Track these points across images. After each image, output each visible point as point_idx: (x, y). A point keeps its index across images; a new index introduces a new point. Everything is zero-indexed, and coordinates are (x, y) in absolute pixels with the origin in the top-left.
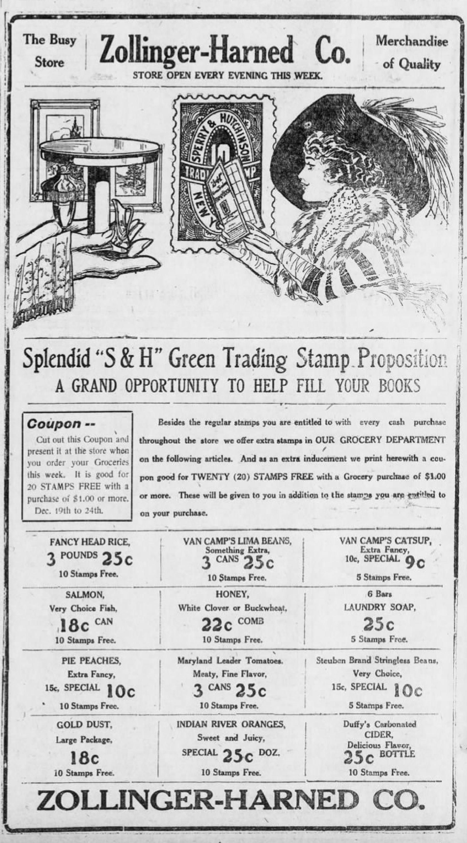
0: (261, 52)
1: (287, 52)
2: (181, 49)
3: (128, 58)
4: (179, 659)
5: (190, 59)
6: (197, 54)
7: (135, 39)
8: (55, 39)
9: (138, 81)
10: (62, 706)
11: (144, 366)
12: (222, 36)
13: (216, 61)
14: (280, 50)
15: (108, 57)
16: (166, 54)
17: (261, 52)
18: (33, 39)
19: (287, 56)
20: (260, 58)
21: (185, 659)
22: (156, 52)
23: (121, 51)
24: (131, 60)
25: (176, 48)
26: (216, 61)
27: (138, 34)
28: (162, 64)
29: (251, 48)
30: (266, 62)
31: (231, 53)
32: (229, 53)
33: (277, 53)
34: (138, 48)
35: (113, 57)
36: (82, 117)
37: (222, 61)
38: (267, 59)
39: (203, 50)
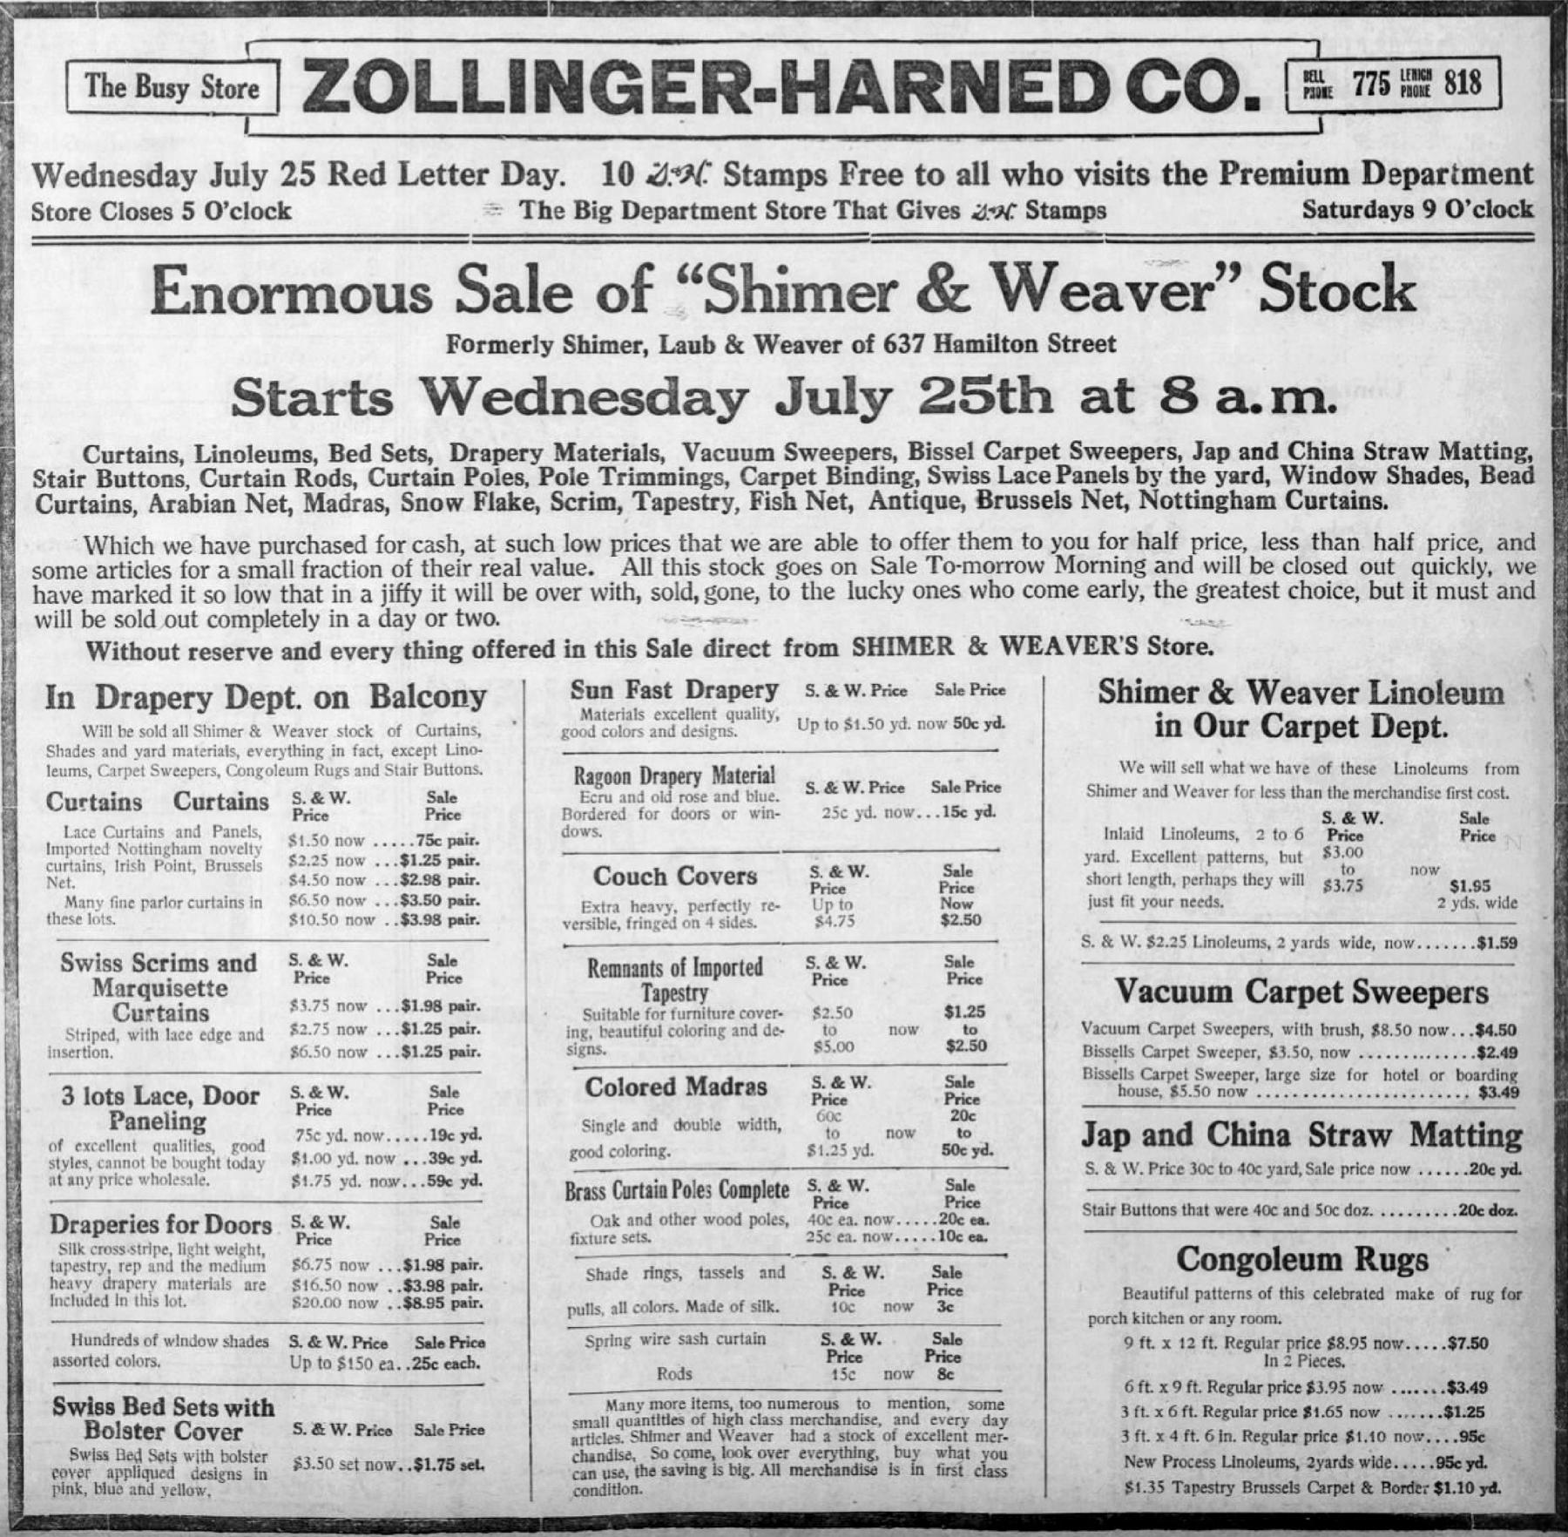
7: (981, 168)
8: (384, 695)
11: (564, 413)
18: (105, 84)
36: (71, 66)
37: (575, 413)
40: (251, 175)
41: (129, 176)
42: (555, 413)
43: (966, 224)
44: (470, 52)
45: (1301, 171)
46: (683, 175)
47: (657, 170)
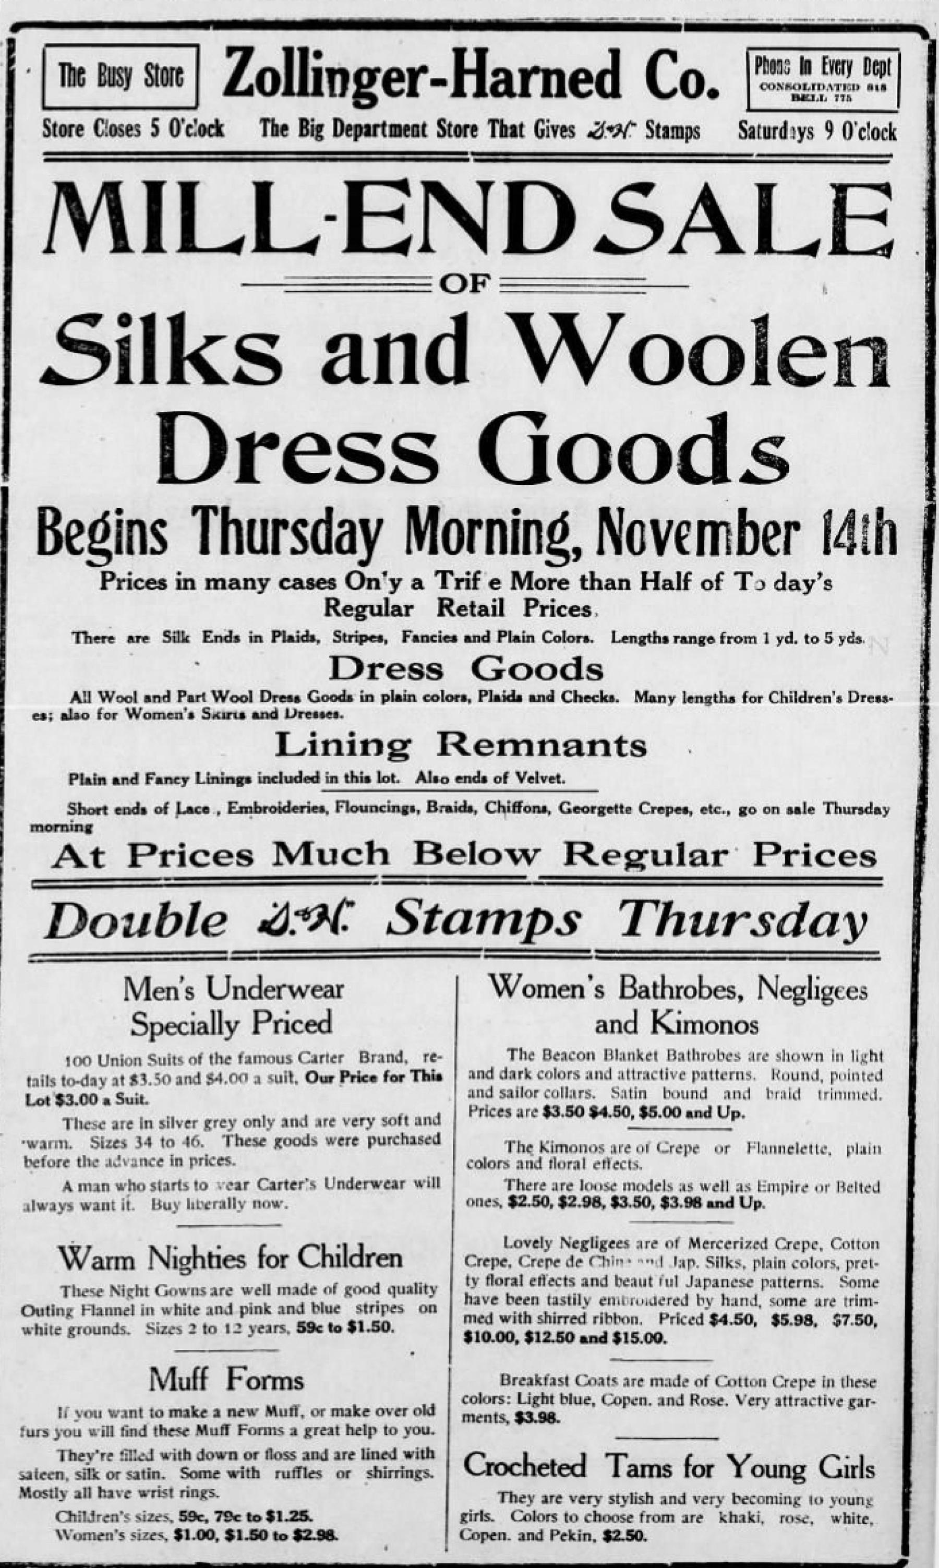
0: (554, 79)
1: (608, 79)
2: (390, 72)
3: (282, 88)
4: (637, 693)
5: (406, 91)
6: (423, 82)
7: (297, 56)
13: (464, 95)
14: (595, 75)
15: (242, 86)
17: (554, 79)
19: (608, 87)
20: (554, 90)
21: (649, 694)
23: (268, 77)
24: (289, 92)
25: (378, 70)
27: (304, 45)
29: (536, 70)
30: (564, 95)
31: (495, 79)
32: (490, 80)
33: (589, 79)
35: (251, 86)
38: (567, 90)
39: (433, 74)
40: (225, 1026)
41: (323, 448)
43: (581, 144)
44: (766, 173)
45: (516, 523)
46: (314, 918)
47: (277, 910)
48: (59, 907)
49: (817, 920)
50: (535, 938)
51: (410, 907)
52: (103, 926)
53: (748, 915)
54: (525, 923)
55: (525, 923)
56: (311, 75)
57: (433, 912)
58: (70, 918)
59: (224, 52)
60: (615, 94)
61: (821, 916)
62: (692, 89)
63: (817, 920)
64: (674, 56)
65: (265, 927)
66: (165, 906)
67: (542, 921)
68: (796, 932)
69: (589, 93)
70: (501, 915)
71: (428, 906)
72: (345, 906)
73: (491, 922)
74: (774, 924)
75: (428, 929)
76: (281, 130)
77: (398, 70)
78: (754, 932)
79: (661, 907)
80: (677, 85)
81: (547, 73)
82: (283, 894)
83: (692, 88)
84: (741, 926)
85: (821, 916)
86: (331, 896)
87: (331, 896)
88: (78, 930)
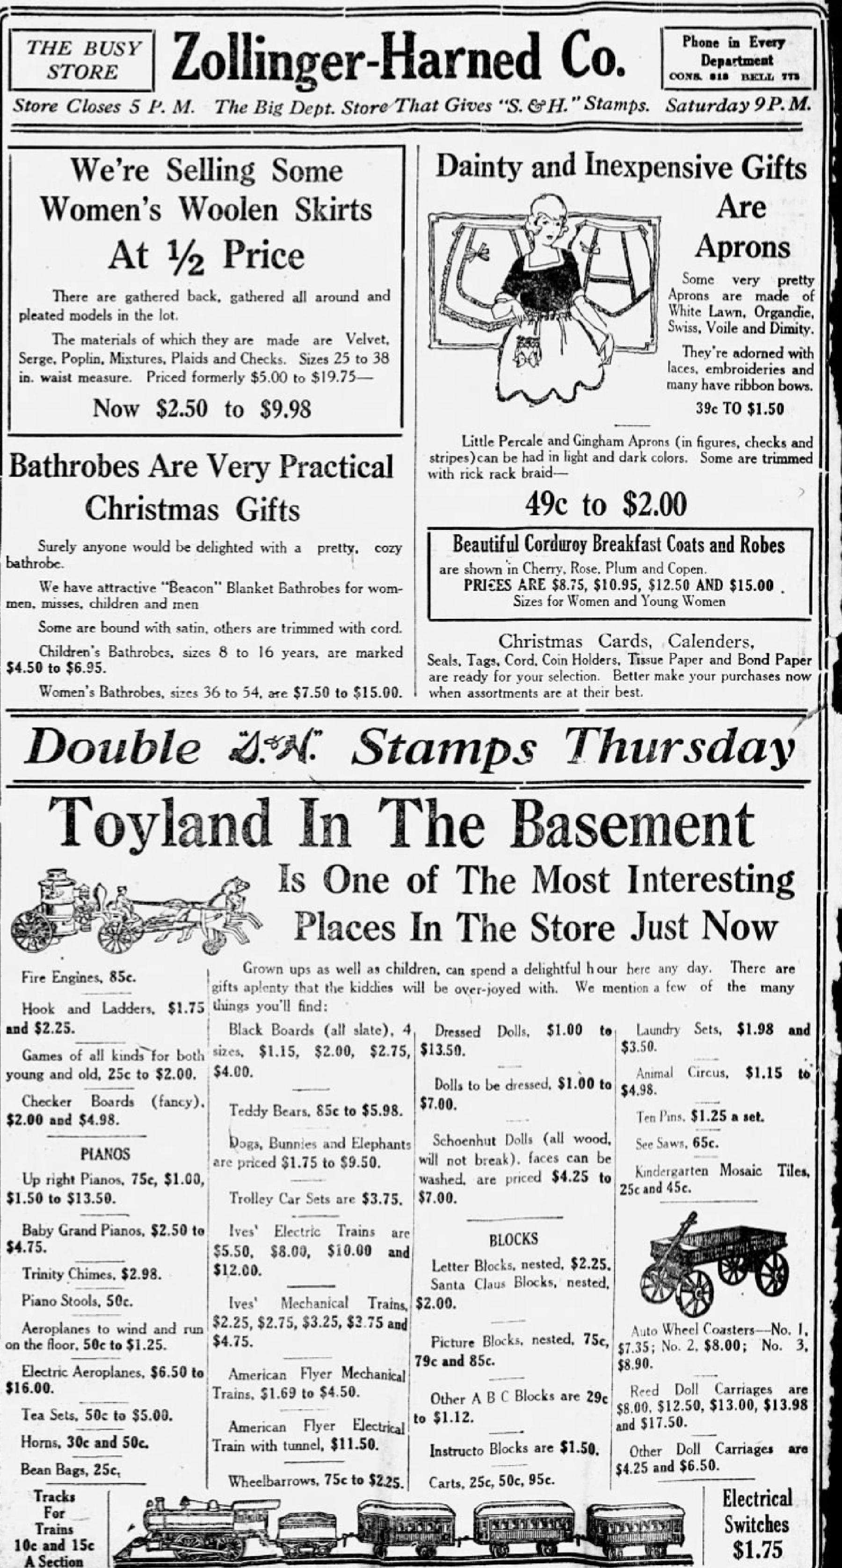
0: (480, 59)
1: (528, 60)
2: (328, 57)
6: (360, 65)
9: (528, 1227)
10: (18, 1546)
11: (393, 77)
12: (405, 33)
14: (515, 58)
15: (188, 71)
16: (300, 66)
17: (480, 59)
20: (480, 70)
22: (281, 62)
23: (213, 60)
24: (234, 76)
25: (318, 55)
26: (392, 77)
28: (292, 84)
29: (461, 51)
30: (489, 77)
31: (421, 61)
32: (418, 62)
33: (510, 62)
34: (247, 52)
35: (197, 70)
37: (404, 77)
39: (369, 58)
42: (448, 76)
48: (40, 732)
49: (746, 745)
50: (492, 768)
51: (375, 737)
52: (81, 752)
53: (680, 742)
54: (483, 754)
55: (483, 754)
56: (254, 59)
57: (397, 742)
58: (49, 744)
59: (173, 36)
60: (535, 75)
61: (749, 741)
62: (604, 67)
63: (746, 745)
64: (586, 34)
65: (236, 755)
66: (141, 733)
67: (499, 750)
68: (726, 758)
69: (511, 75)
70: (462, 744)
71: (392, 736)
72: (313, 734)
73: (452, 752)
74: (705, 750)
75: (392, 760)
76: (235, 108)
77: (338, 56)
78: (686, 759)
79: (604, 734)
80: (590, 63)
81: (473, 55)
82: (251, 725)
83: (604, 66)
84: (677, 752)
85: (749, 741)
86: (299, 728)
87: (299, 728)
88: (57, 755)
